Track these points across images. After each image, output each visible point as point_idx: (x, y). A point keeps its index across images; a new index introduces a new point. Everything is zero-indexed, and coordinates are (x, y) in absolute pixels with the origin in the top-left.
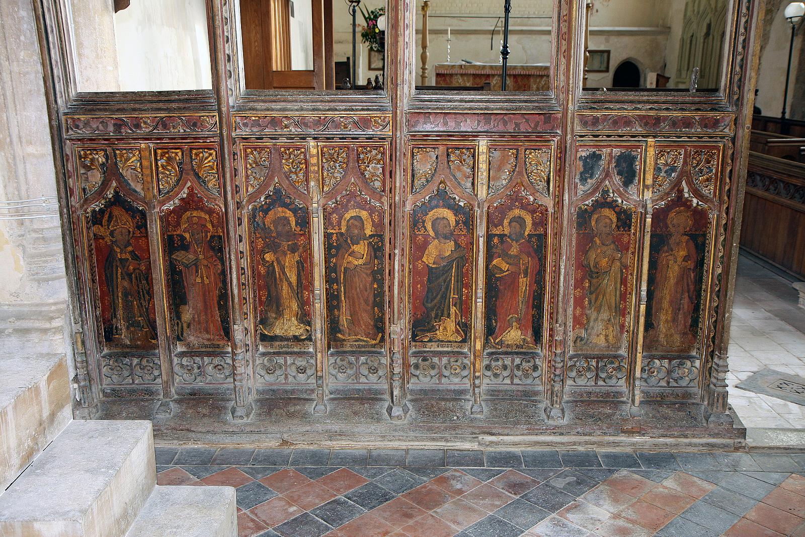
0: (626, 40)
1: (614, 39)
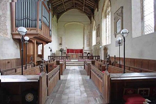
0: (88, 51)
1: (87, 51)
